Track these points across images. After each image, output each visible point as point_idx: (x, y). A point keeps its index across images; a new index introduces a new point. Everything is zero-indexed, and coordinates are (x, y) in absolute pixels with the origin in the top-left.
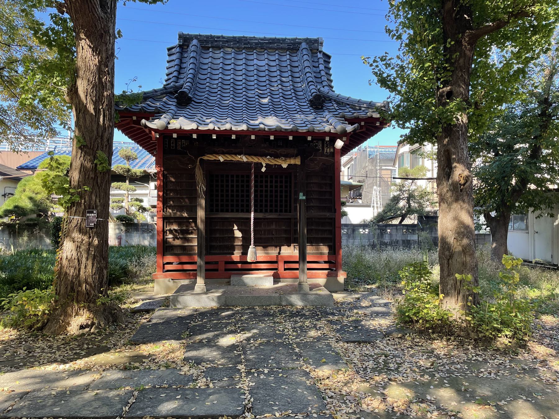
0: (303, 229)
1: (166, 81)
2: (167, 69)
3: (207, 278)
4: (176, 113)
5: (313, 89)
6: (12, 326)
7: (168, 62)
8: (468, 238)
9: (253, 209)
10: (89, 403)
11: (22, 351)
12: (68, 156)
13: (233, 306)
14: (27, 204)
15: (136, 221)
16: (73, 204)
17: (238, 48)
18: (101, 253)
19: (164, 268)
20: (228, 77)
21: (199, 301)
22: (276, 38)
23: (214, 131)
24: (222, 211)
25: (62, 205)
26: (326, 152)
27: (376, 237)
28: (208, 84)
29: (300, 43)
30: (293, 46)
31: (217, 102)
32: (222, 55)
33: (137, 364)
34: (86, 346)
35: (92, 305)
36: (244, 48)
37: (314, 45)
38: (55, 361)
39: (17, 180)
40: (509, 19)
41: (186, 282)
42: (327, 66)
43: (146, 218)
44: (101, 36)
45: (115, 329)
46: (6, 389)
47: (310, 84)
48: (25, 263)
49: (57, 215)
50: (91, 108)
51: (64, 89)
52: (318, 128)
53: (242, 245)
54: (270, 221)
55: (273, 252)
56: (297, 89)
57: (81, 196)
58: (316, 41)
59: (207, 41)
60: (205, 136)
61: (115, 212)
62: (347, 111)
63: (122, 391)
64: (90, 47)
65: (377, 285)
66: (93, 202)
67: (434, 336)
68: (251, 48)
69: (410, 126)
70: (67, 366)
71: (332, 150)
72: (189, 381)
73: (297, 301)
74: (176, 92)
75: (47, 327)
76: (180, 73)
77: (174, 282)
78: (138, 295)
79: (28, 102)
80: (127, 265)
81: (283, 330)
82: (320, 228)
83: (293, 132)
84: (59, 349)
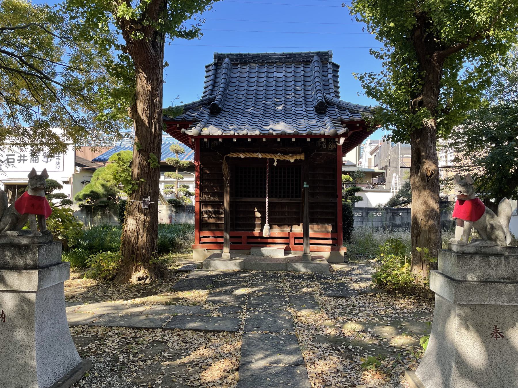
0: (305, 210)
1: (204, 93)
2: (205, 83)
3: (231, 249)
4: (208, 121)
5: (320, 97)
6: (92, 277)
7: (206, 77)
8: (432, 219)
9: (267, 195)
10: (142, 320)
11: (100, 292)
12: (130, 151)
13: (250, 270)
14: (100, 190)
15: (183, 204)
16: (134, 191)
17: (261, 63)
18: (153, 226)
19: (200, 241)
20: (252, 89)
21: (226, 266)
22: (292, 53)
23: (234, 136)
24: (245, 196)
25: (126, 192)
26: (330, 148)
27: (388, 220)
28: (235, 95)
29: (313, 56)
30: (306, 59)
31: (241, 111)
32: (248, 69)
33: (174, 302)
34: (141, 291)
35: (146, 264)
36: (266, 63)
37: (324, 58)
38: (122, 298)
39: (93, 170)
40: (469, 42)
41: (217, 252)
42: (335, 74)
43: (192, 201)
44: (153, 69)
45: (162, 282)
46: (91, 312)
47: (318, 92)
48: (100, 235)
49: (122, 199)
50: (146, 121)
51: (129, 109)
52: (317, 131)
53: (261, 224)
54: (283, 205)
55: (287, 229)
56: (307, 96)
57: (139, 185)
58: (327, 54)
59: (236, 59)
60: (227, 139)
61: (167, 196)
62: (346, 114)
63: (163, 316)
64: (145, 78)
65: (376, 259)
66: (147, 190)
67: (400, 295)
68: (272, 62)
69: (392, 128)
70: (129, 302)
71: (335, 146)
72: (206, 313)
73: (302, 269)
74: (209, 103)
75: (116, 279)
76: (214, 87)
77: (208, 252)
78: (182, 261)
79: (103, 119)
80: (174, 238)
81: (283, 287)
82: (325, 211)
83: (296, 135)
84: (124, 292)
